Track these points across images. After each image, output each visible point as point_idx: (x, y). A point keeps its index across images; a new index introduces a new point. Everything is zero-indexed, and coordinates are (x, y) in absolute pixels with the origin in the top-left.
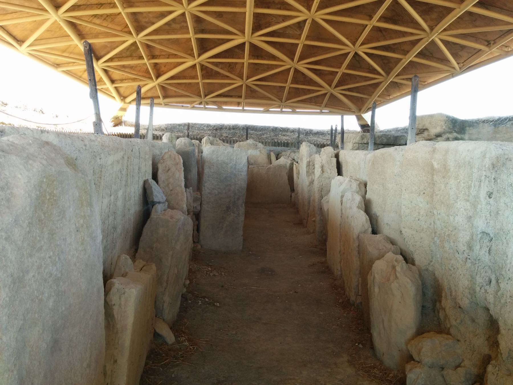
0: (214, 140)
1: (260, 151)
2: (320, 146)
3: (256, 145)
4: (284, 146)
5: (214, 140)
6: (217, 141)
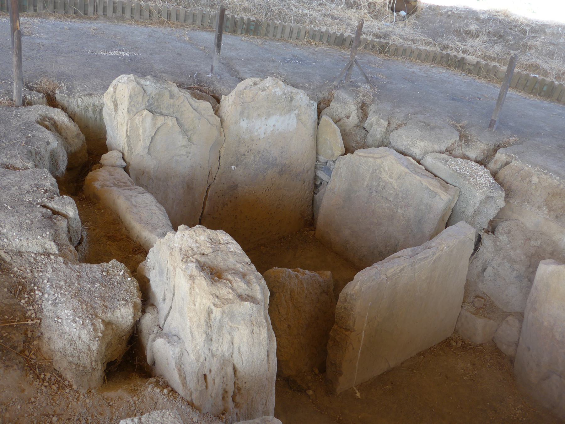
0: (161, 95)
1: (298, 116)
2: (333, 39)
3: (292, 100)
4: (248, 31)
5: (161, 95)
6: (172, 96)
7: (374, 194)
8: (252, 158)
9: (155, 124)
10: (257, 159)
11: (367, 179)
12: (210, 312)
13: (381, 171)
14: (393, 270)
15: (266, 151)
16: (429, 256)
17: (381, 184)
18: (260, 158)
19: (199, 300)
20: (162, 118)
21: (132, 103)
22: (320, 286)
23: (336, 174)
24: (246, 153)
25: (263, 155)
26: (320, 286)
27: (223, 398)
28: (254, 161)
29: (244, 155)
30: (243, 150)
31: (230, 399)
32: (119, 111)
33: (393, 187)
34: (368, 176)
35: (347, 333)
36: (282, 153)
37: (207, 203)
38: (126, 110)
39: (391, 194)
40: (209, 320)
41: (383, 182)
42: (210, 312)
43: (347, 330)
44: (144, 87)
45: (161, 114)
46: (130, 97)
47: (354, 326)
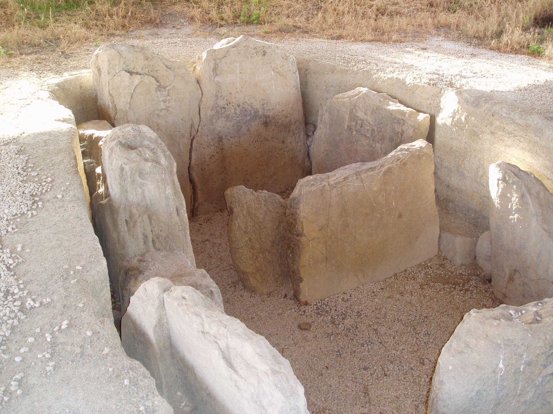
7: (355, 133)
8: (233, 111)
9: (133, 82)
10: (238, 112)
11: (347, 120)
12: (122, 169)
13: (357, 110)
14: (335, 178)
15: (245, 104)
16: (375, 168)
17: (359, 122)
18: (241, 110)
19: (114, 162)
20: (138, 76)
21: (111, 66)
22: (282, 206)
23: (321, 121)
24: (226, 106)
25: (243, 108)
26: (282, 206)
27: (145, 243)
28: (235, 113)
29: (224, 108)
30: (222, 103)
31: (150, 244)
32: (102, 75)
33: (369, 123)
34: (347, 116)
35: (298, 238)
36: (263, 105)
37: (193, 154)
38: (106, 73)
39: (368, 130)
40: (123, 175)
41: (360, 120)
42: (122, 169)
43: (298, 235)
44: (120, 52)
45: (137, 73)
46: (109, 61)
47: (303, 230)
